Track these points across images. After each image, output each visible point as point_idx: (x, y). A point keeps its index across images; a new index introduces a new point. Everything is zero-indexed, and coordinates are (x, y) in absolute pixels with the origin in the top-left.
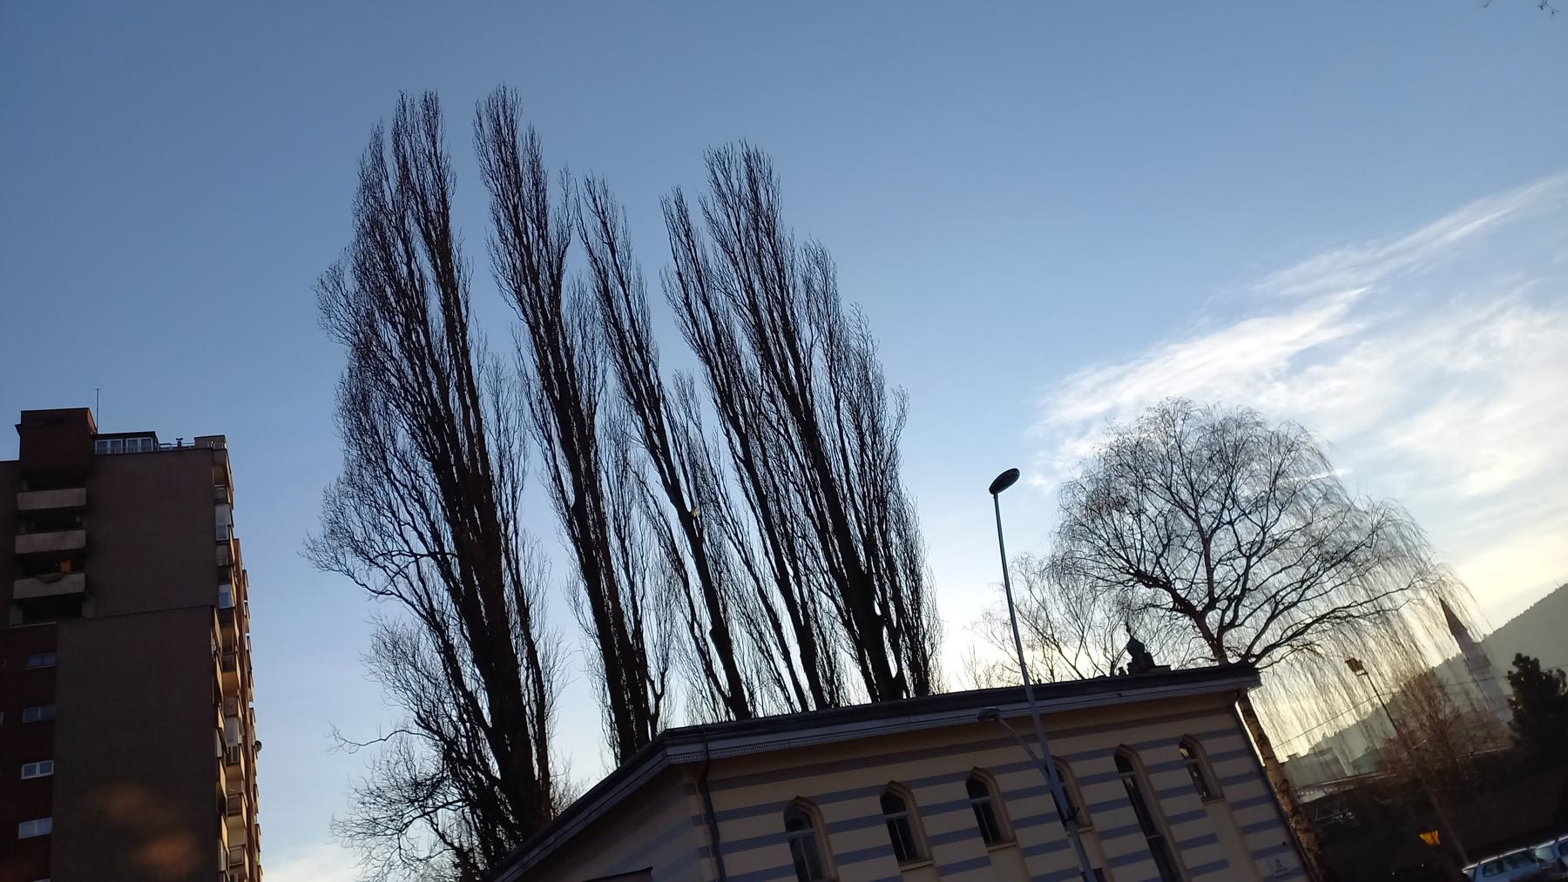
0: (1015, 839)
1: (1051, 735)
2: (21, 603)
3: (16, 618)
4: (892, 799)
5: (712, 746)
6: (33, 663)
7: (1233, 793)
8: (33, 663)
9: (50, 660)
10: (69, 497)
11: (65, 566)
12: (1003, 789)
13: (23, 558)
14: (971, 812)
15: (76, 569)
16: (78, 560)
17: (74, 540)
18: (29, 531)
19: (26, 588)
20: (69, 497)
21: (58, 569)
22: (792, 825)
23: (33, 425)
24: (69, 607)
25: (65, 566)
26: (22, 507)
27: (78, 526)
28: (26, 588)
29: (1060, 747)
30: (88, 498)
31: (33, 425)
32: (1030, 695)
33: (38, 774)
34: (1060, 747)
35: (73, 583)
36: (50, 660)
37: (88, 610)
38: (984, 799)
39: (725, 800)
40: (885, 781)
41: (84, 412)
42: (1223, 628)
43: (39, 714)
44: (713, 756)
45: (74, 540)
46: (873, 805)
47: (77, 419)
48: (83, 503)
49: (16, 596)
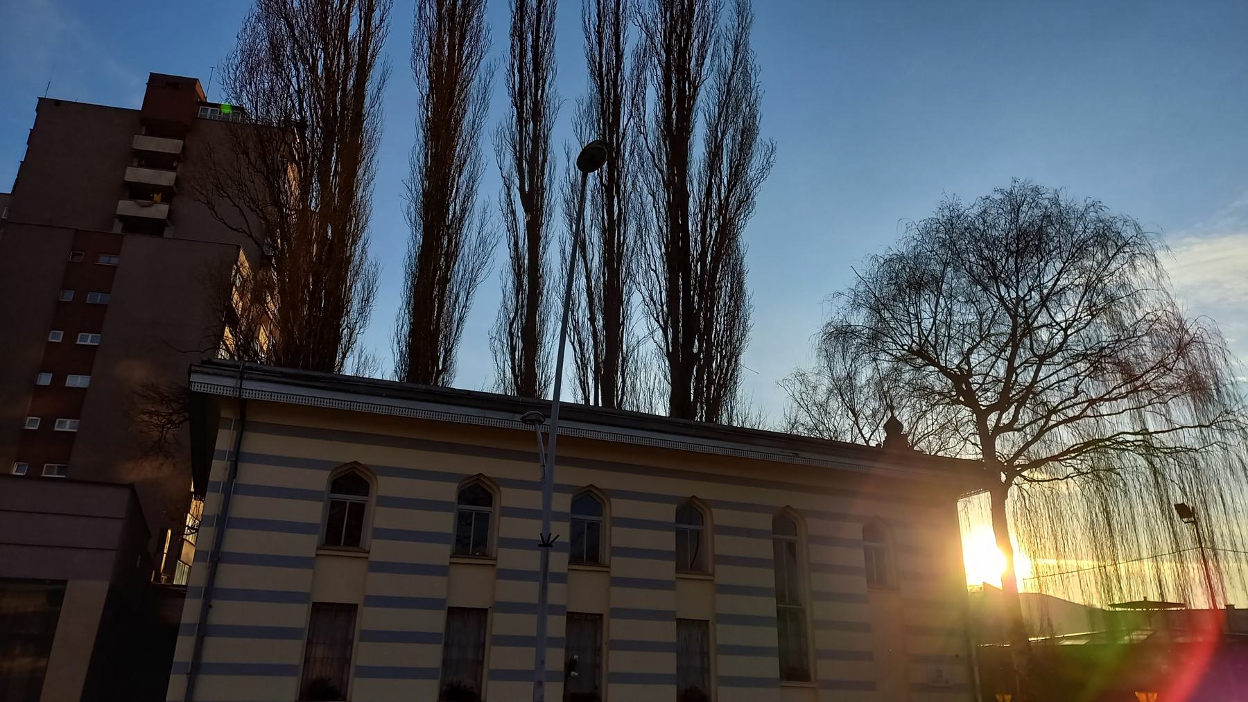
0: (713, 575)
1: (561, 461)
2: (123, 218)
3: (118, 228)
4: (690, 512)
5: (246, 384)
6: (103, 260)
7: (508, 558)
8: (103, 260)
9: (114, 261)
10: (170, 146)
11: (157, 197)
12: (505, 503)
13: (129, 185)
14: (671, 536)
15: (163, 201)
16: (168, 194)
17: (166, 178)
18: (140, 166)
19: (127, 207)
20: (170, 146)
21: (152, 199)
22: (463, 497)
23: (159, 85)
24: (155, 228)
25: (157, 197)
26: (136, 146)
27: (174, 169)
28: (127, 207)
29: (603, 480)
30: (184, 148)
31: (159, 85)
32: (555, 412)
33: (88, 343)
34: (603, 480)
35: (159, 211)
36: (114, 261)
37: (168, 233)
38: (698, 528)
39: (257, 443)
40: (348, 459)
41: (195, 81)
42: (999, 429)
43: (98, 298)
44: (246, 395)
45: (166, 178)
46: (668, 513)
47: (187, 87)
48: (179, 151)
49: (118, 212)
